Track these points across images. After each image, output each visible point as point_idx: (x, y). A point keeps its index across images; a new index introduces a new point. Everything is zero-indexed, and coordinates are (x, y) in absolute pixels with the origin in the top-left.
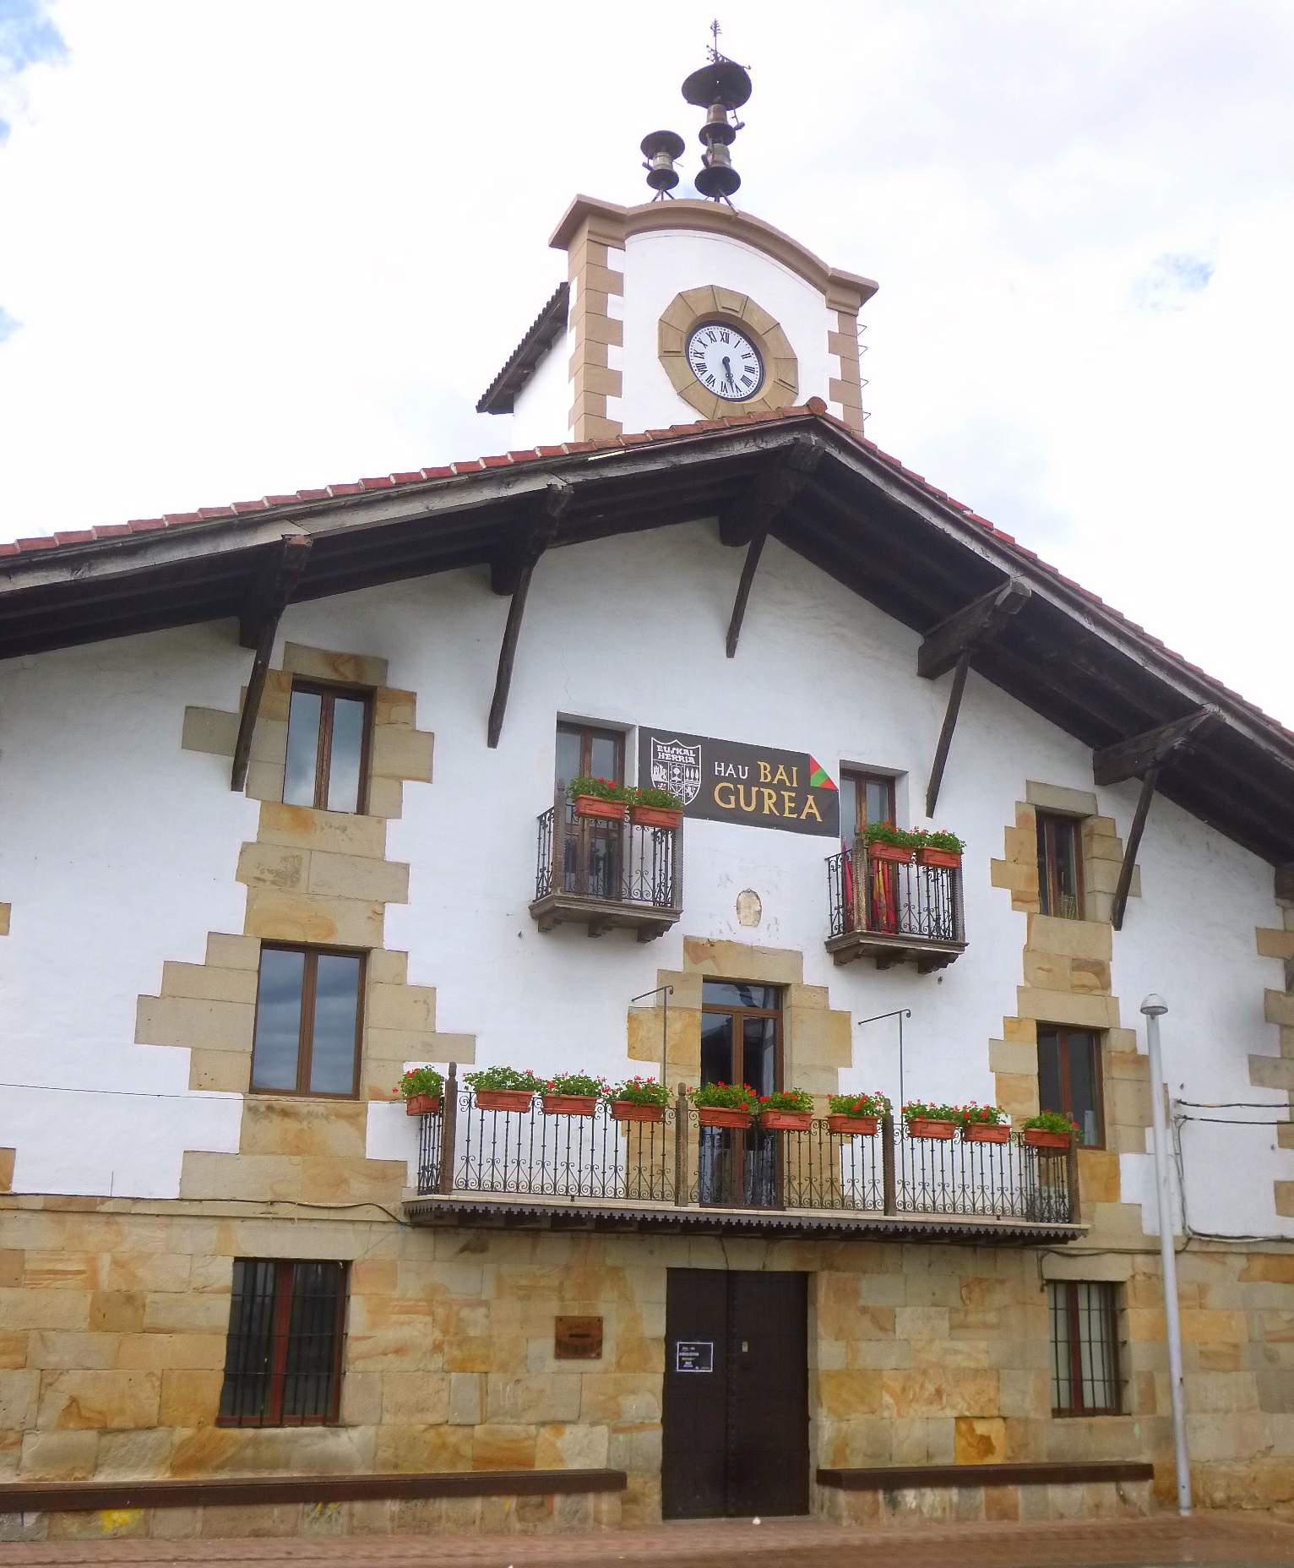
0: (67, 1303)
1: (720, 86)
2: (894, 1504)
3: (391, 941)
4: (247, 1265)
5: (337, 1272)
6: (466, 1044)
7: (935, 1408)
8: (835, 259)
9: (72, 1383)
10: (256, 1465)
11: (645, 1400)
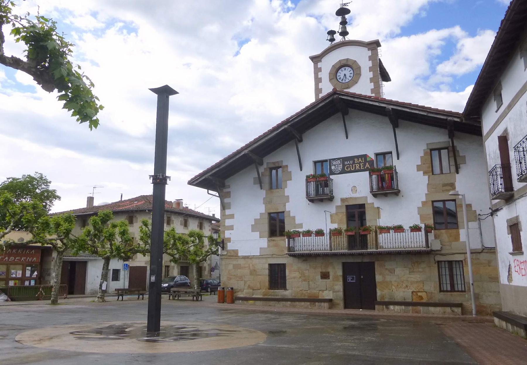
0: (247, 271)
1: (343, 12)
2: (388, 308)
3: (287, 210)
4: (271, 265)
5: (284, 265)
6: (301, 226)
7: (406, 289)
8: (367, 40)
9: (248, 283)
10: (274, 296)
11: (339, 286)
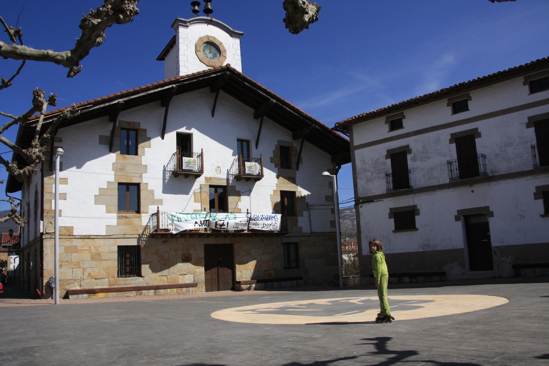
9: (89, 270)
